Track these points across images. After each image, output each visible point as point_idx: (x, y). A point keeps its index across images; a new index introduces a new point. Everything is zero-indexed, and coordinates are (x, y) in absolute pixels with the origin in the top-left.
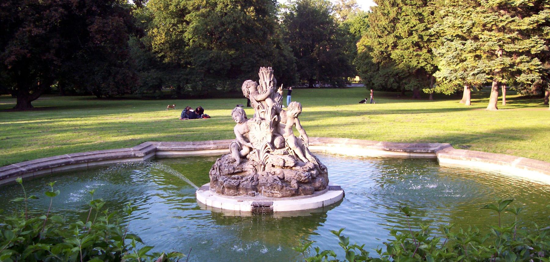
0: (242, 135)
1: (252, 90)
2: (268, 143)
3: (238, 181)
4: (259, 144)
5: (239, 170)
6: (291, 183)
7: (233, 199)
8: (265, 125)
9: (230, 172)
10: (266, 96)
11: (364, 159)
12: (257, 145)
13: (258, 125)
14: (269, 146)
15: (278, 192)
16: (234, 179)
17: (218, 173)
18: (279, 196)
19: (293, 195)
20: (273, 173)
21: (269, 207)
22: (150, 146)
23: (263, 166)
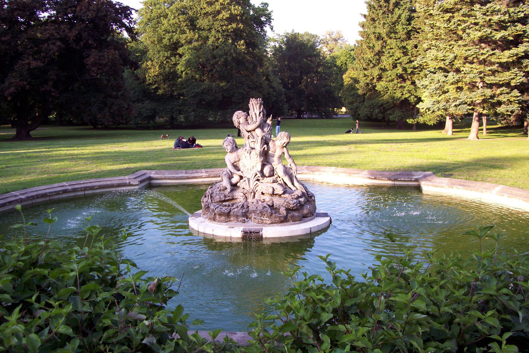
0: (233, 164)
1: (242, 120)
2: (258, 171)
3: (229, 208)
4: (249, 172)
5: (230, 198)
6: (280, 210)
7: (224, 225)
8: (255, 154)
9: (221, 200)
10: (256, 126)
11: (351, 187)
12: (247, 173)
13: (248, 154)
14: (259, 175)
15: (268, 219)
16: (226, 206)
17: (210, 200)
18: (268, 222)
19: (282, 222)
20: (263, 201)
21: (259, 233)
22: (144, 174)
23: (253, 194)
